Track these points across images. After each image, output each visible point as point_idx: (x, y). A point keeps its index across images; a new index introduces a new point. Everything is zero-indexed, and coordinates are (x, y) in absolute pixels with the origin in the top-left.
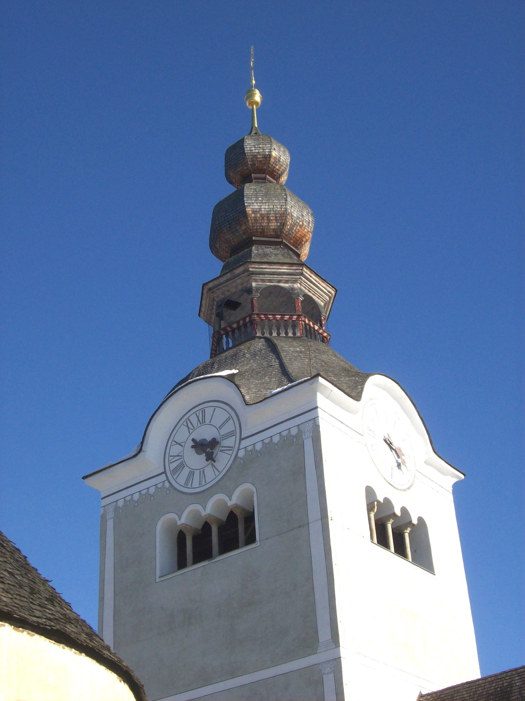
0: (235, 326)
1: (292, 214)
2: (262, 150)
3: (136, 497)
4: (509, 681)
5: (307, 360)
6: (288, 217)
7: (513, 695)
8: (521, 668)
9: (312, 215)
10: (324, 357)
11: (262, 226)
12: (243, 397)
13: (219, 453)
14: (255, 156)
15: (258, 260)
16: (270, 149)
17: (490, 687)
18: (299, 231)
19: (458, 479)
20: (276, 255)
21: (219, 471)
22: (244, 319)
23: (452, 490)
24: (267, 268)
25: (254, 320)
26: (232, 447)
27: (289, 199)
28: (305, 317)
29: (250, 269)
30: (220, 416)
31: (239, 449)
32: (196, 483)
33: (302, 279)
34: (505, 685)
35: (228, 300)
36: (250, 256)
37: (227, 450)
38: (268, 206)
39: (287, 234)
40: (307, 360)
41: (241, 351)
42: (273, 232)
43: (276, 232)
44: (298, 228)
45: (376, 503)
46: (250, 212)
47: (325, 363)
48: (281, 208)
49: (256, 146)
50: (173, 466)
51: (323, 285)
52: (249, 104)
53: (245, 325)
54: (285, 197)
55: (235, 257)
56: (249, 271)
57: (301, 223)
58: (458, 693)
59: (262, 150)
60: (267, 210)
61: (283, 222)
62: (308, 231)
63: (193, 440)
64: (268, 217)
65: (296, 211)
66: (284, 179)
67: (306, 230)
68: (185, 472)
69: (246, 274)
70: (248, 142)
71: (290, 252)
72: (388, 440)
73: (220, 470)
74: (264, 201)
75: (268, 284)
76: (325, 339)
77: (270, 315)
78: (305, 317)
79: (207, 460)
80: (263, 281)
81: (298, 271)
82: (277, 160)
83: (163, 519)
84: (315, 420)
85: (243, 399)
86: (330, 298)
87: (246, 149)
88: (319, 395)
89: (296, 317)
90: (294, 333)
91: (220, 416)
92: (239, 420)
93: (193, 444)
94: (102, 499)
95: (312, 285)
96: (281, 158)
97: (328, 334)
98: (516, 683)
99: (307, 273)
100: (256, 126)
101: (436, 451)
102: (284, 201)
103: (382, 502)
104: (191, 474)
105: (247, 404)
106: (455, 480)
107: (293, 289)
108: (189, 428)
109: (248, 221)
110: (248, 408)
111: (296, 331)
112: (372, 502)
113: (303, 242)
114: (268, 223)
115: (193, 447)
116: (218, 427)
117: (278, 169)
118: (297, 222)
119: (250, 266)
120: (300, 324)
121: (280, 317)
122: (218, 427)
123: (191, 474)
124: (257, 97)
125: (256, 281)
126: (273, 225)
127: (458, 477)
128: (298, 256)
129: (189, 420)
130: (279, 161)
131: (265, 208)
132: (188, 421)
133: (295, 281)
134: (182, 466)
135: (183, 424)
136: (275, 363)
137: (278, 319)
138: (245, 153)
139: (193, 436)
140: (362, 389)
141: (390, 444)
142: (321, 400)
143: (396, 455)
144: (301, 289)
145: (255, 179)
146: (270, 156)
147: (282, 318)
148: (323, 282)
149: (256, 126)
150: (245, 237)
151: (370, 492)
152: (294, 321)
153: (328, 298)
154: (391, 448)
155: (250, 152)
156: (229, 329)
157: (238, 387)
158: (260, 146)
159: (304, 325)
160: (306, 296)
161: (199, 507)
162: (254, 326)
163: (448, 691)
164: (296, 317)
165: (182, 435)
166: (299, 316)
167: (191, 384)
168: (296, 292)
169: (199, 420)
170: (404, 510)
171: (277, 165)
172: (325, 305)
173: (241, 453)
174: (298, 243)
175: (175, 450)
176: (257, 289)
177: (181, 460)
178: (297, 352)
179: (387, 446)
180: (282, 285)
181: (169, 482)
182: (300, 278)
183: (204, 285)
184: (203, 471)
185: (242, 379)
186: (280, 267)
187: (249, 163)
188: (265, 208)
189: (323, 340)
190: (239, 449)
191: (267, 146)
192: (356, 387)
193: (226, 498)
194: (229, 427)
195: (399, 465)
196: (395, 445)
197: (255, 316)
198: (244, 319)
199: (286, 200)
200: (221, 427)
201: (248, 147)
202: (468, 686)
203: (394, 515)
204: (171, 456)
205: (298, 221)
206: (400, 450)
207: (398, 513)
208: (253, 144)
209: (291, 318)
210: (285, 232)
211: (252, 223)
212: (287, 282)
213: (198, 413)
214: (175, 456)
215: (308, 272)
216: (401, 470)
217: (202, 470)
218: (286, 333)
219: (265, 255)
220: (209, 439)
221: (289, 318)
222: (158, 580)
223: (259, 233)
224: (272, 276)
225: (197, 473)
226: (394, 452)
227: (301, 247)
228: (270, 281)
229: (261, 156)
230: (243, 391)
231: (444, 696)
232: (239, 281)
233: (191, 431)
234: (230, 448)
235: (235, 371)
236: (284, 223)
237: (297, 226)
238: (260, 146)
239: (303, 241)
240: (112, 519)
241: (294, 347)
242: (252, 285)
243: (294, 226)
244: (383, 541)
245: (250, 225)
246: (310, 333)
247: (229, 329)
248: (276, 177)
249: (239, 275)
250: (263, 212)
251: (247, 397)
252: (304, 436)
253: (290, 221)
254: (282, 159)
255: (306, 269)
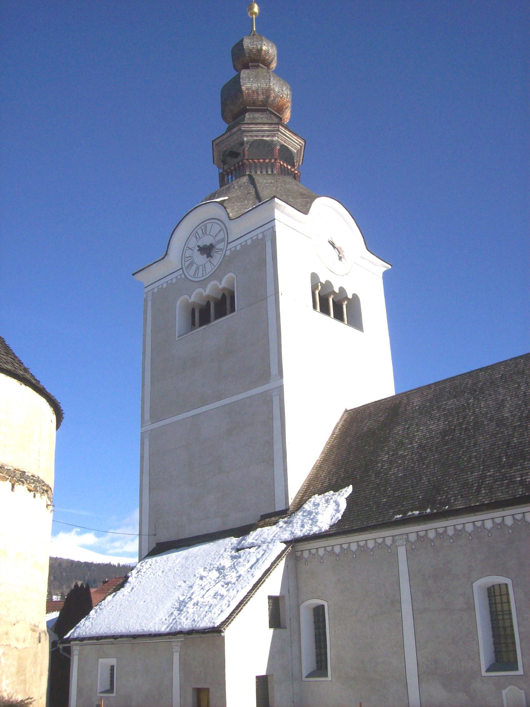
0: (232, 168)
1: (274, 90)
2: (255, 46)
3: (165, 285)
4: (400, 400)
5: (274, 188)
6: (272, 91)
7: (400, 409)
8: (409, 391)
9: (290, 90)
10: (288, 186)
11: (253, 99)
12: (228, 214)
13: (215, 253)
14: (251, 51)
15: (249, 122)
16: (261, 45)
17: (388, 404)
18: (280, 101)
19: (386, 268)
20: (262, 118)
21: (214, 266)
22: (238, 163)
23: (383, 276)
24: (254, 127)
25: (245, 163)
26: (222, 249)
27: (272, 79)
28: (280, 160)
29: (242, 129)
30: (216, 228)
31: (226, 250)
32: (200, 274)
33: (279, 134)
34: (397, 402)
35: (230, 151)
36: (244, 120)
37: (219, 251)
38: (257, 84)
39: (271, 103)
40: (274, 188)
41: (232, 184)
42: (261, 102)
43: (263, 103)
44: (279, 99)
45: (319, 284)
46: (245, 89)
47: (288, 190)
48: (266, 85)
49: (252, 43)
50: (187, 264)
51: (294, 138)
52: (250, 14)
53: (239, 167)
54: (269, 77)
55: (235, 121)
56: (241, 130)
57: (281, 96)
58: (368, 409)
59: (255, 46)
60: (256, 87)
61: (268, 95)
62: (287, 101)
63: (198, 246)
64: (257, 92)
65: (277, 87)
66: (274, 65)
67: (285, 100)
68: (194, 267)
69: (239, 132)
70: (246, 41)
71: (272, 116)
72: (332, 242)
73: (215, 265)
74: (254, 81)
75: (255, 138)
76: (296, 175)
77: (256, 159)
78: (280, 160)
79: (207, 257)
80: (251, 136)
81: (276, 128)
82: (267, 52)
83: (181, 299)
84: (273, 227)
85: (227, 216)
86: (301, 147)
87: (244, 46)
88: (276, 210)
89: (273, 160)
90: (272, 172)
91: (216, 228)
92: (227, 230)
93: (198, 249)
94: (145, 288)
95: (287, 138)
96: (270, 51)
97: (298, 172)
98: (404, 401)
99: (282, 130)
100: (255, 29)
101: (368, 249)
102: (268, 80)
103: (324, 283)
104: (198, 268)
105: (230, 220)
106: (385, 269)
107: (272, 141)
108: (197, 238)
109: (243, 96)
110: (232, 222)
111: (274, 170)
112: (317, 284)
113: (284, 109)
114: (258, 96)
115: (198, 250)
116: (214, 236)
117: (267, 59)
118: (278, 95)
119: (242, 126)
120: (276, 165)
121: (262, 160)
122: (214, 236)
123: (198, 268)
124: (256, 9)
125: (246, 136)
126: (261, 97)
127: (386, 267)
128: (281, 119)
129: (197, 232)
130: (268, 53)
131: (255, 86)
132: (196, 234)
133: (274, 136)
134: (192, 263)
135: (193, 236)
136: (253, 191)
137: (261, 162)
138: (244, 49)
139: (198, 244)
140: (310, 207)
141: (333, 245)
142: (278, 214)
143: (338, 252)
144: (278, 141)
145: (252, 66)
146: (261, 49)
147: (264, 161)
148: (294, 136)
149: (255, 29)
150: (242, 107)
151: (314, 277)
152: (273, 163)
153: (299, 147)
154: (334, 247)
155: (247, 47)
156: (229, 171)
157: (225, 208)
158: (254, 43)
159: (279, 166)
160: (282, 146)
161: (201, 290)
162: (245, 168)
163: (363, 408)
164: (273, 160)
165: (193, 243)
166: (276, 160)
167: (198, 208)
168: (275, 143)
169: (203, 232)
170: (342, 289)
171: (266, 56)
172: (297, 151)
173: (228, 253)
174: (280, 109)
175: (188, 253)
176: (248, 142)
177: (191, 260)
178: (268, 183)
179: (331, 246)
180: (265, 138)
181: (184, 274)
182: (277, 133)
183: (213, 142)
184: (205, 265)
185: (229, 203)
186: (263, 126)
187: (247, 55)
188: (255, 86)
189: (295, 177)
190: (226, 250)
191: (259, 43)
192: (306, 205)
193: (218, 283)
194: (221, 236)
195: (340, 258)
196: (337, 245)
197: (245, 161)
198: (238, 163)
199: (270, 80)
200: (216, 236)
201: (246, 44)
202: (375, 403)
203: (334, 292)
204: (186, 257)
205: (279, 94)
206: (341, 249)
207: (337, 291)
208: (249, 42)
209: (270, 161)
210: (270, 102)
211: (246, 97)
212: (268, 136)
213: (202, 227)
214: (188, 257)
215: (283, 129)
216: (342, 261)
217: (204, 265)
218: (267, 172)
219: (254, 118)
220: (208, 244)
221: (269, 161)
222: (177, 339)
223: (251, 104)
224: (257, 133)
225: (201, 268)
226: (336, 249)
227: (283, 113)
228: (257, 136)
229: (255, 50)
230: (228, 210)
231: (359, 410)
232: (235, 137)
233: (198, 240)
234: (221, 250)
235: (226, 198)
236: (268, 96)
237: (279, 98)
238: (254, 43)
239: (283, 108)
240: (151, 301)
241: (267, 180)
242: (244, 140)
243: (276, 98)
244: (325, 310)
245: (245, 98)
246: (284, 172)
247: (229, 171)
248: (267, 64)
249: (235, 133)
250: (253, 89)
251: (231, 215)
252: (266, 239)
253: (273, 94)
254: (271, 51)
255: (282, 127)
